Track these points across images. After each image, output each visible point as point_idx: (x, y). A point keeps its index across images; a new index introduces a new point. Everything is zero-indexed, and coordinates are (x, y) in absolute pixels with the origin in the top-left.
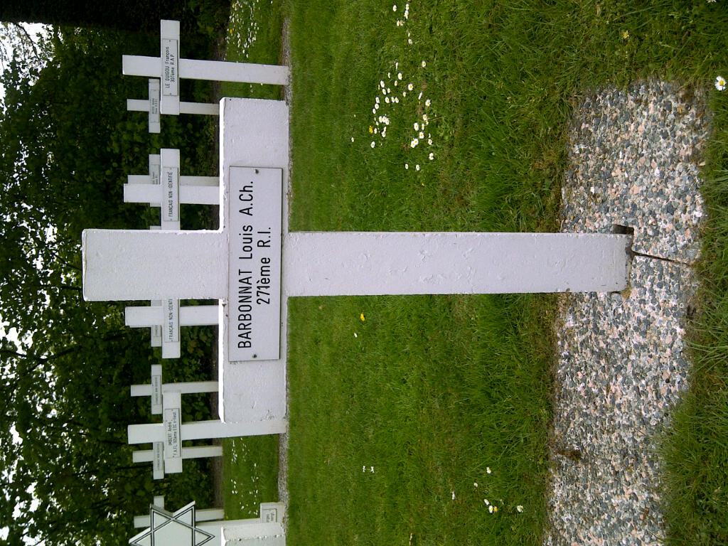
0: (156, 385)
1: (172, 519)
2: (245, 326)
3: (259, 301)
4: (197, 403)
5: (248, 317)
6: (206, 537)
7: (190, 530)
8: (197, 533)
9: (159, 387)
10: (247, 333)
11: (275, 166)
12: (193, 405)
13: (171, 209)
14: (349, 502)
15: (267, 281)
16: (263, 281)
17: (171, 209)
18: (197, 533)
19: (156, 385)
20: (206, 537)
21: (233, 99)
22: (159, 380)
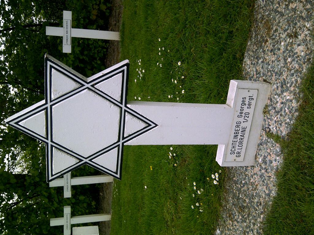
0: (67, 28)
1: (87, 85)
2: (241, 142)
3: (245, 117)
4: (96, 61)
5: (238, 133)
6: (143, 125)
7: (117, 110)
8: (128, 117)
9: (69, 30)
10: (243, 135)
11: (255, 88)
12: (93, 63)
13: (67, 227)
14: (193, 25)
15: (244, 101)
16: (249, 105)
17: (67, 227)
18: (128, 117)
19: (67, 28)
20: (143, 125)
21: (203, 144)
22: (69, 216)
